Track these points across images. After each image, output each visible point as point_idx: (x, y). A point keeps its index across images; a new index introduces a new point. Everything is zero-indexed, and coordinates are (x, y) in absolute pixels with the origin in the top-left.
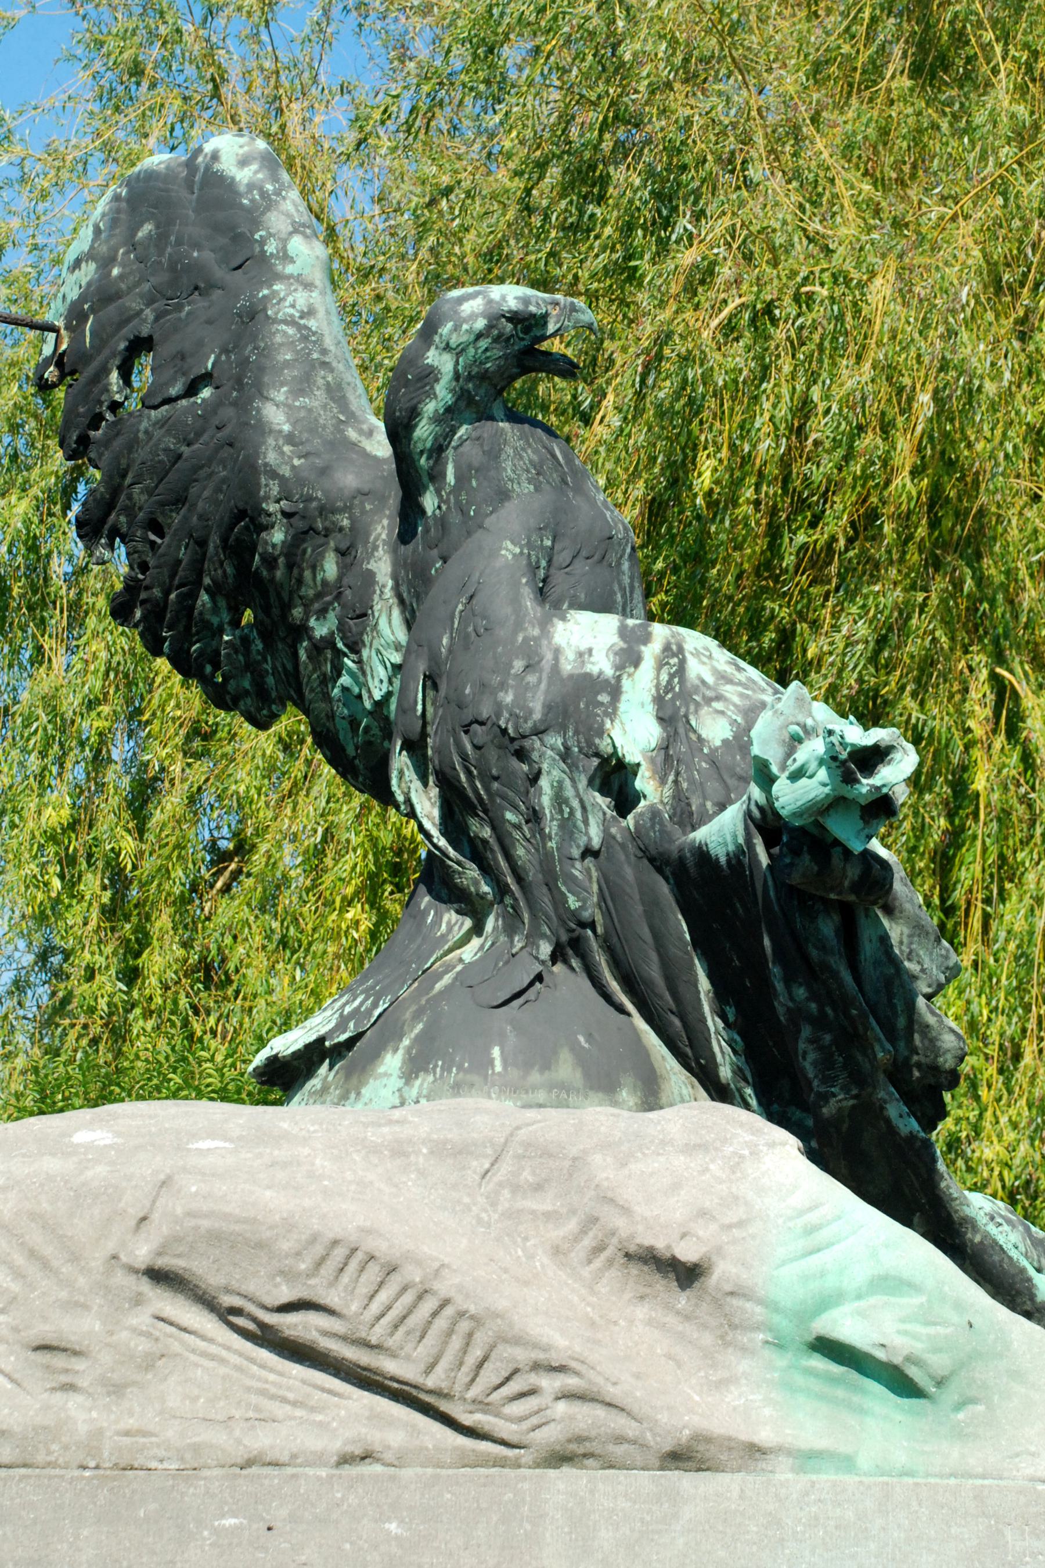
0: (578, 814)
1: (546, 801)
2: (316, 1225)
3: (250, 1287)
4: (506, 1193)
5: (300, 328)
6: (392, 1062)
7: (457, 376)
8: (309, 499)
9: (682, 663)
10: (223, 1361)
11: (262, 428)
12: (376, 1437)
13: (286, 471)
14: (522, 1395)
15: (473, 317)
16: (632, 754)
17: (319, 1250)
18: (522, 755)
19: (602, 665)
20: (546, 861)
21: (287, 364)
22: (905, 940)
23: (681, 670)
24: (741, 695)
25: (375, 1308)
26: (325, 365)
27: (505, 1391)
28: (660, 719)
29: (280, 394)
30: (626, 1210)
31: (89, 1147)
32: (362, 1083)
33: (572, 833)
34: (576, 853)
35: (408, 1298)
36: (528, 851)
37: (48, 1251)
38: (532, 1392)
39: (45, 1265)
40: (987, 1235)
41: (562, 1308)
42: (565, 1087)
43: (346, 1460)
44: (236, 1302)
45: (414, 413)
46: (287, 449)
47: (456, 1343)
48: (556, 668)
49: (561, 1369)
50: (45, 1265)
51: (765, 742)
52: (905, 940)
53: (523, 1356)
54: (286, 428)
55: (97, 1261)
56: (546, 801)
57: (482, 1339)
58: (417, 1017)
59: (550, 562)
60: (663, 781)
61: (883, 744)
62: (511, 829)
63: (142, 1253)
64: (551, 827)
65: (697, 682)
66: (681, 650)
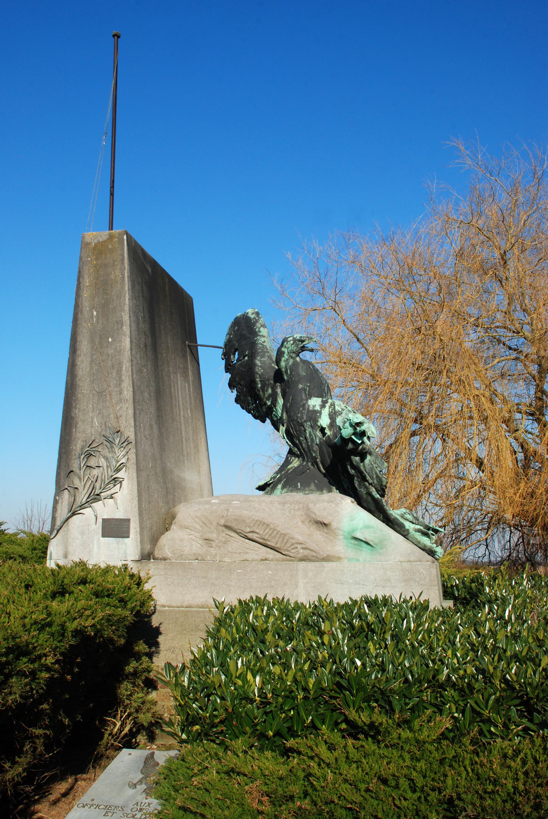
1: (308, 435)
2: (254, 517)
3: (242, 529)
4: (292, 511)
5: (262, 345)
6: (280, 486)
7: (288, 353)
8: (264, 378)
9: (335, 407)
10: (238, 542)
11: (255, 365)
12: (267, 556)
13: (260, 373)
14: (294, 548)
15: (290, 341)
16: (324, 426)
17: (254, 522)
18: (303, 426)
19: (318, 408)
20: (308, 446)
23: (334, 408)
25: (265, 533)
26: (268, 352)
27: (291, 548)
28: (330, 418)
29: (259, 358)
30: (315, 514)
31: (214, 503)
32: (274, 490)
35: (272, 531)
37: (206, 522)
38: (297, 548)
39: (206, 524)
40: (395, 517)
41: (302, 533)
42: (313, 490)
43: (262, 560)
44: (240, 531)
45: (280, 360)
47: (281, 539)
48: (308, 409)
49: (302, 544)
50: (206, 524)
53: (294, 541)
55: (215, 523)
56: (308, 435)
57: (286, 538)
58: (285, 478)
60: (330, 430)
63: (222, 522)
64: (309, 440)
66: (334, 404)
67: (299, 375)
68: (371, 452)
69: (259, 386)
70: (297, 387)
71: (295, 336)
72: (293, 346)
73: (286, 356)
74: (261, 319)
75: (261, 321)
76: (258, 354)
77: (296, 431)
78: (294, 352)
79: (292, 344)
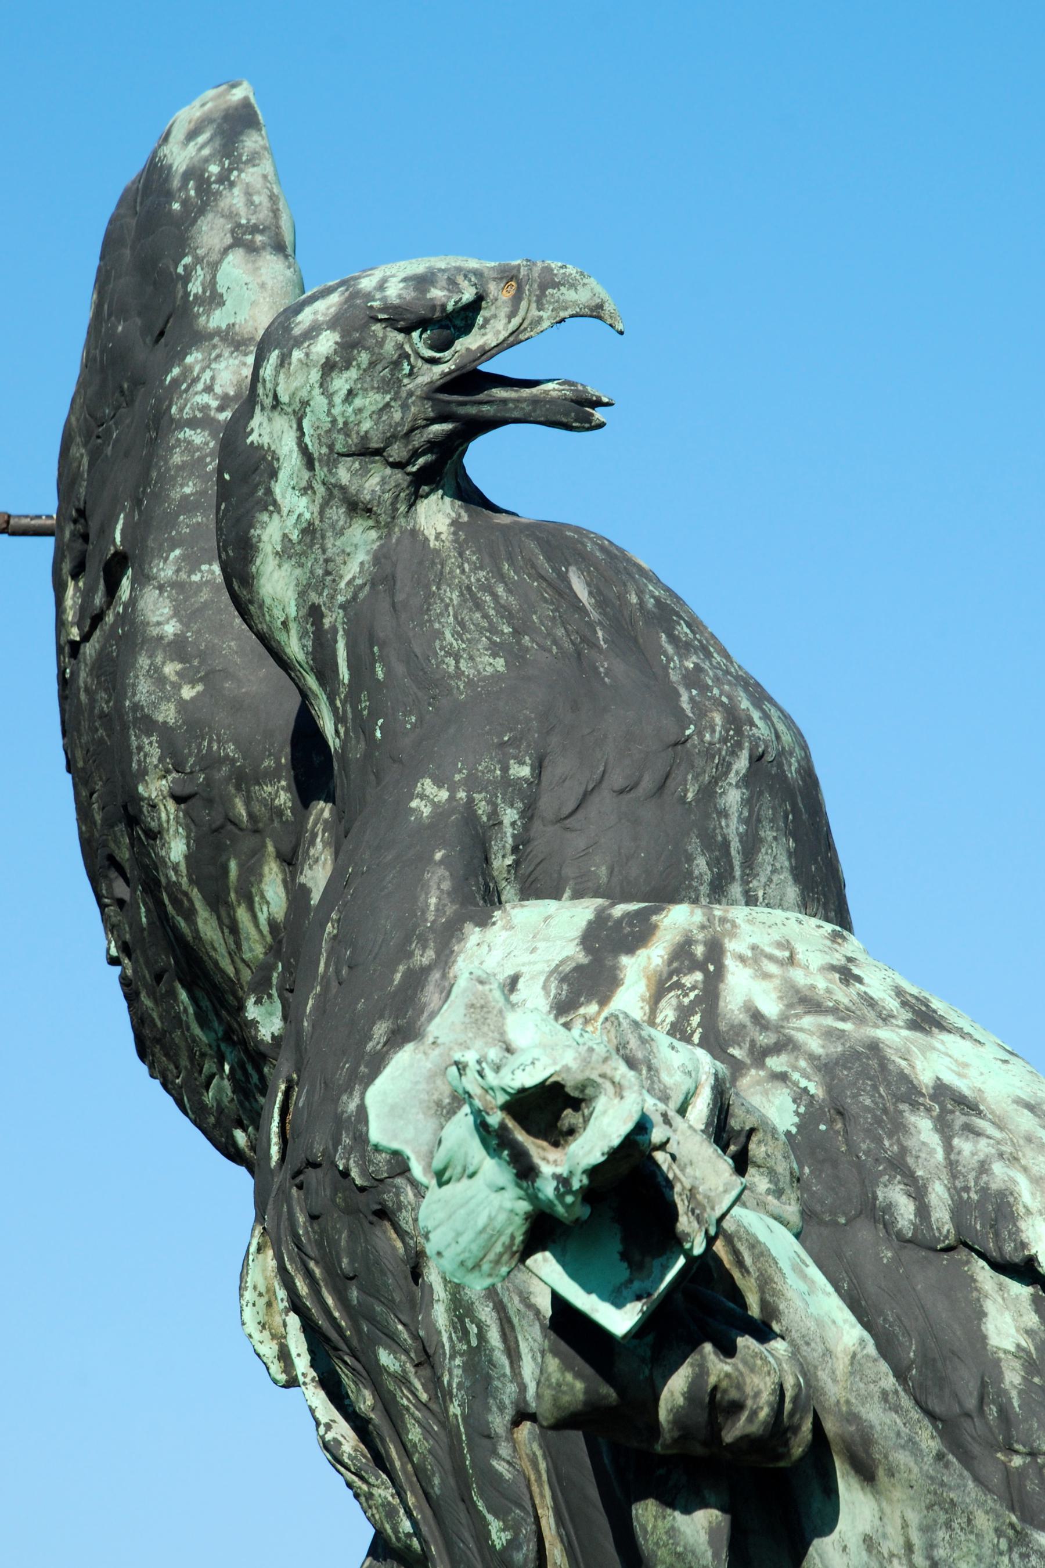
0: (494, 1337)
1: (440, 1315)
8: (210, 763)
9: (714, 981)
13: (167, 714)
21: (187, 505)
22: (916, 1538)
24: (830, 1034)
33: (488, 1379)
34: (498, 1422)
36: (426, 1430)
46: (170, 669)
51: (395, 1112)
52: (916, 1538)
54: (170, 629)
59: (529, 814)
61: (570, 1084)
62: (391, 1386)
64: (454, 1373)
65: (743, 1018)
67: (431, 682)
68: (866, 1438)
69: (177, 849)
70: (402, 809)
71: (367, 284)
72: (341, 383)
73: (292, 502)
74: (250, 176)
75: (249, 191)
76: (171, 522)
77: (340, 1282)
78: (367, 452)
79: (329, 368)
